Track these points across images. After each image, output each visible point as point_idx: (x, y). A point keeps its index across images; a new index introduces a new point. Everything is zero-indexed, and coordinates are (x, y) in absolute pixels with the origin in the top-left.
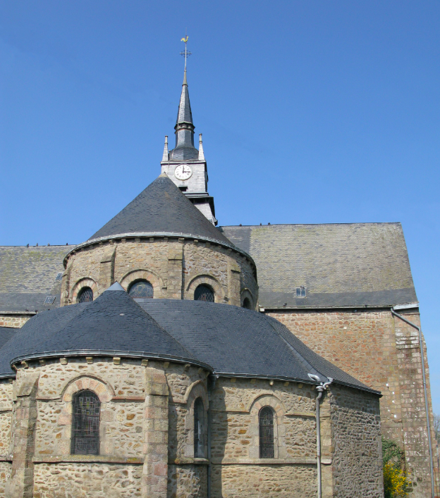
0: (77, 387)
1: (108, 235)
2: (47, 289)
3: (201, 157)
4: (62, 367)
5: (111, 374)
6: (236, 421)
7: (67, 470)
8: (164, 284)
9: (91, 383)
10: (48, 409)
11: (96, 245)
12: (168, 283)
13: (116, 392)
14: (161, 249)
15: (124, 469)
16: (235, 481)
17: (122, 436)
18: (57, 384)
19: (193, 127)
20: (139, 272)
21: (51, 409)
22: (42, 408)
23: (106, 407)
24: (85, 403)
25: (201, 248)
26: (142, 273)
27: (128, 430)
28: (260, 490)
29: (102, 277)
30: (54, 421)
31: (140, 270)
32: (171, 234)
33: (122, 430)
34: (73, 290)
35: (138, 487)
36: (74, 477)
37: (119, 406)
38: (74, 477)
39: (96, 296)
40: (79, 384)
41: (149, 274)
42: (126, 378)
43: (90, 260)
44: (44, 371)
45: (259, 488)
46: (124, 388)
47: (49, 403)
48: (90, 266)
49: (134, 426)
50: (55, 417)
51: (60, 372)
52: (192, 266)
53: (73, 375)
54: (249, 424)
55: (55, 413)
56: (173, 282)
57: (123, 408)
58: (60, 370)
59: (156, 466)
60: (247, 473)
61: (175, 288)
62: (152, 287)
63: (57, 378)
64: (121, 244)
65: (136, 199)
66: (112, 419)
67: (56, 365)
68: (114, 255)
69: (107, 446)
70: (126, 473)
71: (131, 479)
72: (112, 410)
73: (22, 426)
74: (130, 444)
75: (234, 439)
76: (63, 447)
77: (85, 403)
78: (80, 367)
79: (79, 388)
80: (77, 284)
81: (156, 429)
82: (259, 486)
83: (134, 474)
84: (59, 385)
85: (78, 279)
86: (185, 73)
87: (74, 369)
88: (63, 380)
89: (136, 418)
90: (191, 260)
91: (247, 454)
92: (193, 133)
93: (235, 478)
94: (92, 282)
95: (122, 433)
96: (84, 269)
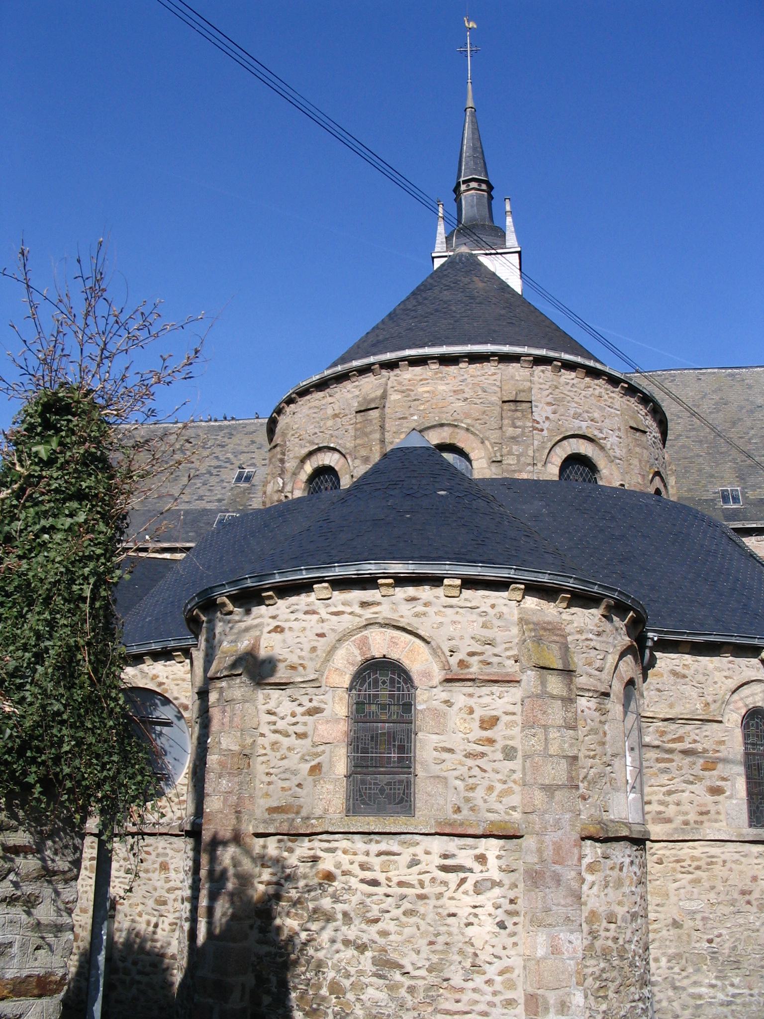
0: (357, 652)
1: (367, 355)
2: (219, 501)
3: (512, 240)
4: (319, 605)
5: (440, 619)
6: (695, 741)
7: (339, 853)
8: (495, 452)
9: (393, 642)
10: (286, 707)
11: (343, 377)
12: (505, 451)
13: (454, 661)
14: (486, 382)
15: (478, 852)
16: (697, 881)
17: (470, 768)
18: (307, 647)
19: (490, 188)
20: (439, 430)
21: (293, 706)
22: (271, 706)
23: (427, 698)
24: (382, 687)
25: (568, 376)
26: (447, 431)
27: (483, 755)
28: (754, 903)
29: (358, 441)
30: (301, 736)
31: (442, 425)
32: (506, 349)
33: (468, 755)
34: (295, 474)
35: (511, 894)
36: (355, 869)
37: (460, 695)
38: (355, 869)
39: (345, 482)
40: (364, 644)
41: (462, 433)
42: (476, 629)
43: (330, 412)
44: (274, 617)
45: (751, 898)
46: (472, 654)
47: (289, 692)
48: (330, 423)
49: (499, 746)
50: (305, 724)
51: (315, 617)
52: (552, 416)
53: (347, 622)
54: (722, 748)
55: (303, 714)
56: (515, 447)
57: (471, 702)
58: (314, 612)
59: (554, 843)
60: (724, 862)
61: (519, 461)
62: (470, 461)
63: (308, 633)
64: (397, 371)
65: (413, 293)
66: (445, 731)
67: (302, 600)
68: (384, 396)
69: (431, 799)
70: (481, 859)
71: (496, 875)
72: (444, 707)
73: (224, 746)
74: (490, 789)
75: (692, 783)
76: (329, 797)
77: (382, 687)
78: (364, 604)
79: (362, 654)
80: (303, 461)
81: (551, 752)
82: (750, 893)
83: (503, 863)
84: (314, 649)
85: (305, 451)
86: (469, 84)
87: (348, 609)
88: (322, 635)
89: (501, 725)
90: (549, 404)
91: (722, 817)
92: (491, 198)
93: (699, 873)
94: (337, 456)
95: (470, 762)
96: (317, 430)
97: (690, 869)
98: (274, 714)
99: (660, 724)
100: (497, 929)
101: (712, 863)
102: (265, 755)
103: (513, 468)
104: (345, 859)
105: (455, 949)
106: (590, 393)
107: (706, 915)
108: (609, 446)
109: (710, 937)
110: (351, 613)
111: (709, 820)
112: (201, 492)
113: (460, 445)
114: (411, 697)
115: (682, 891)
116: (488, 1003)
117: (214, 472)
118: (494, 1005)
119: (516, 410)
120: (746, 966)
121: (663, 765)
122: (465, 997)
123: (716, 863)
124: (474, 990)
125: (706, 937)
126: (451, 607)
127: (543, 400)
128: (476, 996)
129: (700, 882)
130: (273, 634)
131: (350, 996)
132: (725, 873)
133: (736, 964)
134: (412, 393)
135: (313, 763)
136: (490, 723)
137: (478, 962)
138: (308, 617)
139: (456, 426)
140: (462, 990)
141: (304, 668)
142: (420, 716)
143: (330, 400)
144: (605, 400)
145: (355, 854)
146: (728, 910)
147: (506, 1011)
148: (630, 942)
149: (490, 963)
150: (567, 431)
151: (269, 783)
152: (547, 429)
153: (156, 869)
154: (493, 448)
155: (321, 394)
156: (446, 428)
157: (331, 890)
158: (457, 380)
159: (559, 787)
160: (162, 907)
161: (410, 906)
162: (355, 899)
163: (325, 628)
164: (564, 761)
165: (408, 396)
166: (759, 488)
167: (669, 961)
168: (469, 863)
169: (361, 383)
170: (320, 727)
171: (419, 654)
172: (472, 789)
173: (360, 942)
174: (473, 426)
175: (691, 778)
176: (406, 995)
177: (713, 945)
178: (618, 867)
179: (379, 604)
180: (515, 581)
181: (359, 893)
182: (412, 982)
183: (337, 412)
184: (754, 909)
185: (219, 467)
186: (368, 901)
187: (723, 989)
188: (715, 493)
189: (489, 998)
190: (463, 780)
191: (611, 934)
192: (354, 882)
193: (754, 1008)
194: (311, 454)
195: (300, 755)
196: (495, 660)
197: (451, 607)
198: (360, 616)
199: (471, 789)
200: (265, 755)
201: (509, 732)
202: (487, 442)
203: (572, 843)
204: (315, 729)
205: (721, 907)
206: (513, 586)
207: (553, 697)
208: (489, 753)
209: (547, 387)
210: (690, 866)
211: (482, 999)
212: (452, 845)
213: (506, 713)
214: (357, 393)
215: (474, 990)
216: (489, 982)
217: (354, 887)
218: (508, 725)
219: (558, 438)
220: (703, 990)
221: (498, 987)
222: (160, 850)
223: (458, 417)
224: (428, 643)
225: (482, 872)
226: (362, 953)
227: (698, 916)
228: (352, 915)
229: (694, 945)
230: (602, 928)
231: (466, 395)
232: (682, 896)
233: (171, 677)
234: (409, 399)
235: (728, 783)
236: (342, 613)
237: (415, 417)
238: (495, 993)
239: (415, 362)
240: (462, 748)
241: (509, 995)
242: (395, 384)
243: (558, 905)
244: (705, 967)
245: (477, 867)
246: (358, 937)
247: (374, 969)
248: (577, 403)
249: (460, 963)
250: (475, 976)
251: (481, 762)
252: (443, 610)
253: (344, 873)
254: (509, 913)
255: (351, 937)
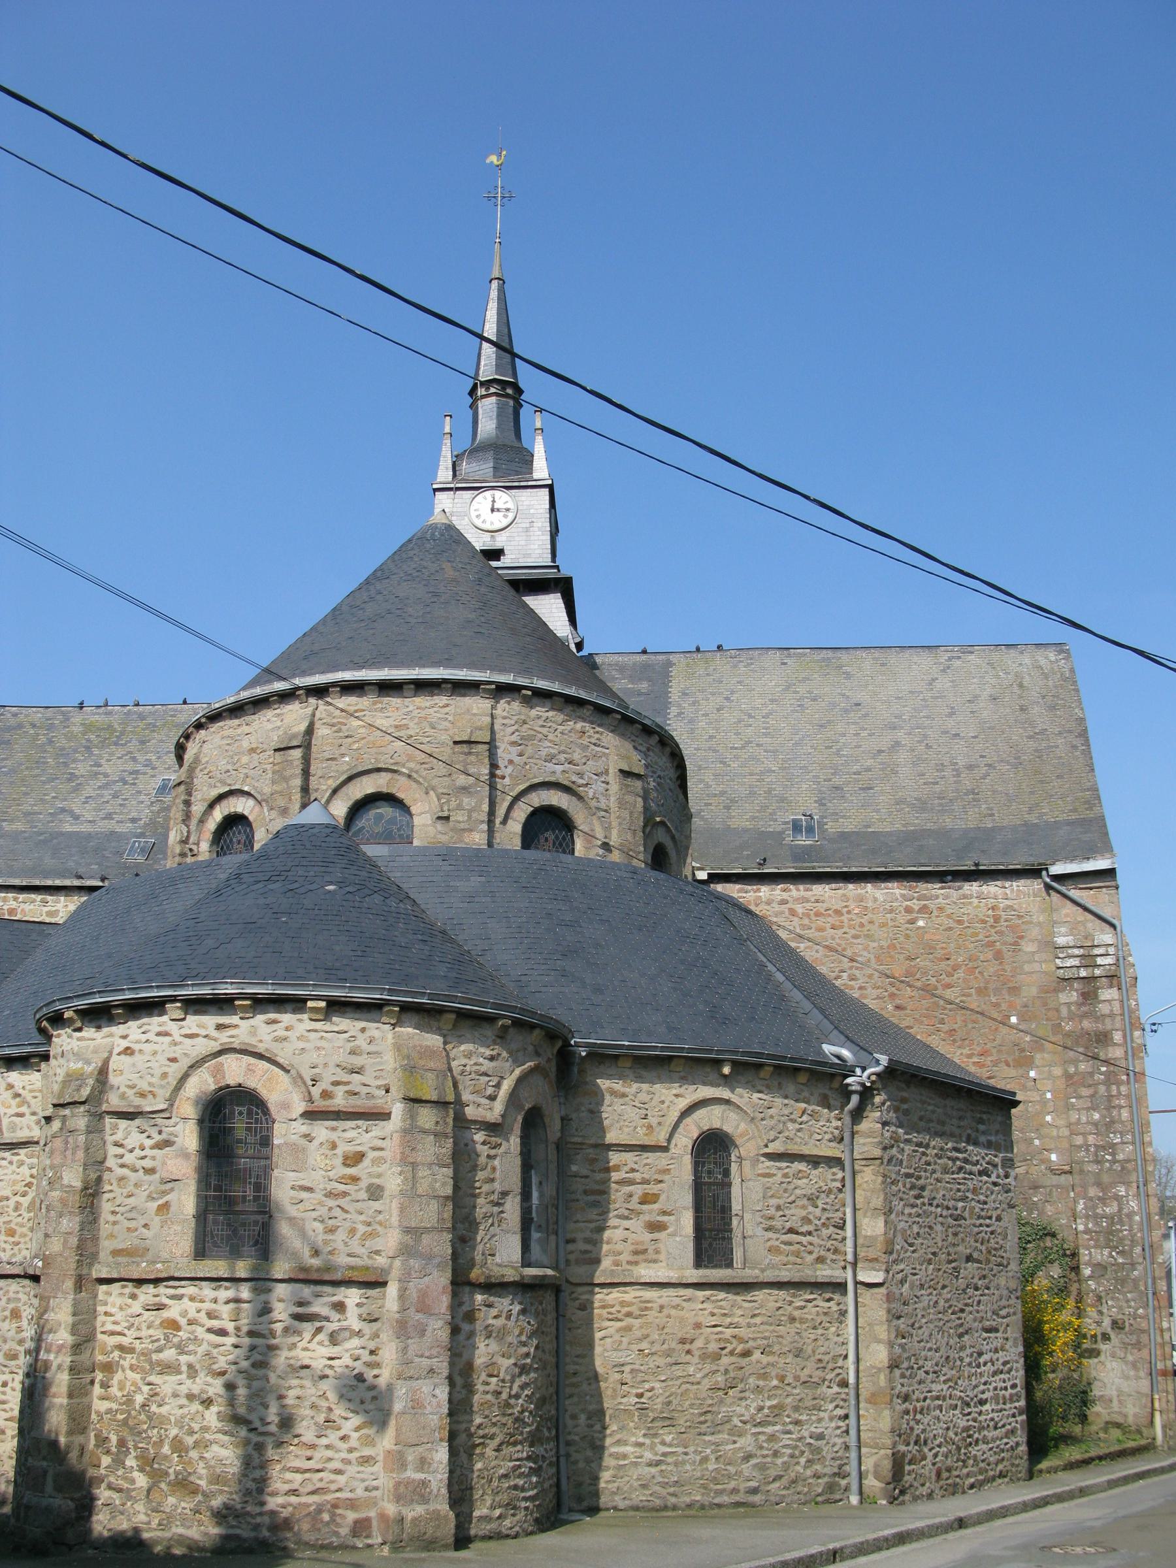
0: (211, 1080)
2: (134, 820)
4: (173, 1027)
5: (301, 1045)
6: (633, 1170)
7: (185, 1300)
9: (250, 1070)
10: (135, 1139)
11: (260, 703)
12: (453, 804)
13: (316, 1092)
14: (434, 715)
15: (335, 1299)
16: (628, 1329)
17: (330, 1209)
18: (158, 1072)
20: (375, 775)
22: (119, 1136)
23: (287, 1131)
25: (540, 711)
29: (276, 788)
30: (150, 1171)
31: (379, 770)
33: (330, 1194)
34: (202, 821)
35: (372, 1345)
37: (322, 1131)
39: (261, 837)
40: (218, 1072)
41: (403, 780)
43: (245, 744)
44: (124, 1037)
46: (336, 1083)
47: (137, 1122)
48: (245, 759)
49: (363, 1184)
50: (154, 1158)
51: (167, 1039)
52: (517, 759)
53: (202, 1047)
54: (666, 1177)
55: (152, 1148)
56: (466, 800)
57: (334, 1136)
58: (167, 1034)
59: (419, 1291)
60: (662, 1307)
61: (470, 817)
63: (158, 1057)
65: (367, 582)
67: (155, 1023)
68: (310, 731)
70: (340, 1307)
71: (356, 1325)
72: (303, 1142)
74: (353, 1231)
75: (627, 1218)
78: (220, 1027)
80: (211, 806)
81: (420, 1191)
82: (692, 1341)
83: (363, 1311)
84: (164, 1075)
88: (173, 1060)
89: (366, 1162)
90: (514, 743)
93: (629, 1320)
94: (251, 802)
95: (331, 1203)
96: (230, 767)
97: (619, 1316)
98: (121, 1146)
99: (591, 1151)
100: (355, 1383)
101: (646, 1309)
102: (111, 1191)
103: (462, 826)
104: (191, 1307)
105: (307, 1403)
106: (569, 728)
107: (636, 1367)
108: (591, 795)
109: (641, 1391)
110: (206, 1036)
111: (646, 1261)
112: (109, 808)
113: (400, 795)
114: (270, 1129)
115: (608, 1340)
116: (343, 1460)
117: (129, 779)
118: (349, 1462)
119: (470, 753)
120: (682, 1422)
121: (591, 1198)
122: (318, 1454)
123: (651, 1309)
124: (327, 1447)
125: (634, 1391)
126: (316, 1031)
127: (506, 739)
128: (329, 1453)
129: (631, 1330)
130: (123, 1056)
131: (194, 1454)
132: (661, 1319)
133: (670, 1421)
134: (344, 728)
135: (160, 1202)
136: (355, 1159)
137: (332, 1417)
138: (160, 1039)
139: (395, 771)
140: (313, 1447)
141: (154, 1096)
142: (276, 1151)
143: (246, 729)
144: (590, 737)
145: (202, 1301)
146: (661, 1361)
147: (362, 1469)
148: (517, 1396)
149: (346, 1419)
150: (535, 777)
151: (115, 1223)
152: (510, 775)
153: (6, 1318)
154: (439, 800)
155: (236, 722)
156: (383, 774)
157: (176, 1340)
158: (400, 713)
159: (427, 1230)
160: (13, 1363)
161: (260, 1358)
162: (201, 1350)
163: (177, 1052)
164: (433, 1201)
165: (339, 731)
166: (843, 817)
167: (589, 1418)
168: (324, 1311)
169: (284, 711)
170: (169, 1162)
171: (277, 1083)
172: (332, 1231)
173: (205, 1396)
174: (417, 772)
175: (626, 1213)
176: (253, 1452)
177: (643, 1400)
178: (504, 1315)
179: (236, 1026)
180: (388, 1003)
181: (205, 1343)
182: (260, 1439)
183: (254, 746)
184: (696, 1360)
185: (137, 772)
186: (215, 1351)
187: (652, 1447)
188: (787, 823)
189: (344, 1455)
190: (322, 1221)
191: (492, 1388)
192: (200, 1332)
193: (688, 1467)
194: (221, 798)
195: (146, 1193)
196: (365, 1090)
197: (316, 1031)
198: (215, 1040)
199: (331, 1231)
200: (111, 1191)
201: (376, 1169)
202: (432, 793)
203: (440, 1289)
204: (164, 1163)
205: (655, 1357)
206: (386, 1009)
207: (425, 1132)
208: (352, 1192)
209: (513, 722)
210: (619, 1312)
211: (336, 1456)
212: (307, 1291)
213: (374, 1149)
214: (279, 724)
215: (327, 1447)
216: (343, 1438)
217: (200, 1337)
218: (376, 1162)
219: (522, 787)
220: (629, 1449)
221: (353, 1443)
222: (11, 1295)
223: (399, 759)
224: (288, 1071)
225: (339, 1320)
226: (207, 1408)
227: (627, 1369)
228: (198, 1367)
229: (620, 1400)
230: (480, 1381)
231: (410, 732)
232: (608, 1347)
233: (28, 1087)
234: (341, 734)
235: (672, 1218)
236: (197, 1035)
237: (347, 759)
238: (351, 1450)
239: (350, 688)
240: (321, 1186)
241: (367, 1452)
242: (323, 716)
243: (422, 1356)
244: (632, 1424)
245: (334, 1316)
246: (203, 1391)
247: (220, 1425)
248: (551, 741)
249: (312, 1418)
250: (329, 1432)
251: (342, 1202)
252: (307, 1034)
253: (191, 1323)
254: (369, 1365)
255: (196, 1391)
